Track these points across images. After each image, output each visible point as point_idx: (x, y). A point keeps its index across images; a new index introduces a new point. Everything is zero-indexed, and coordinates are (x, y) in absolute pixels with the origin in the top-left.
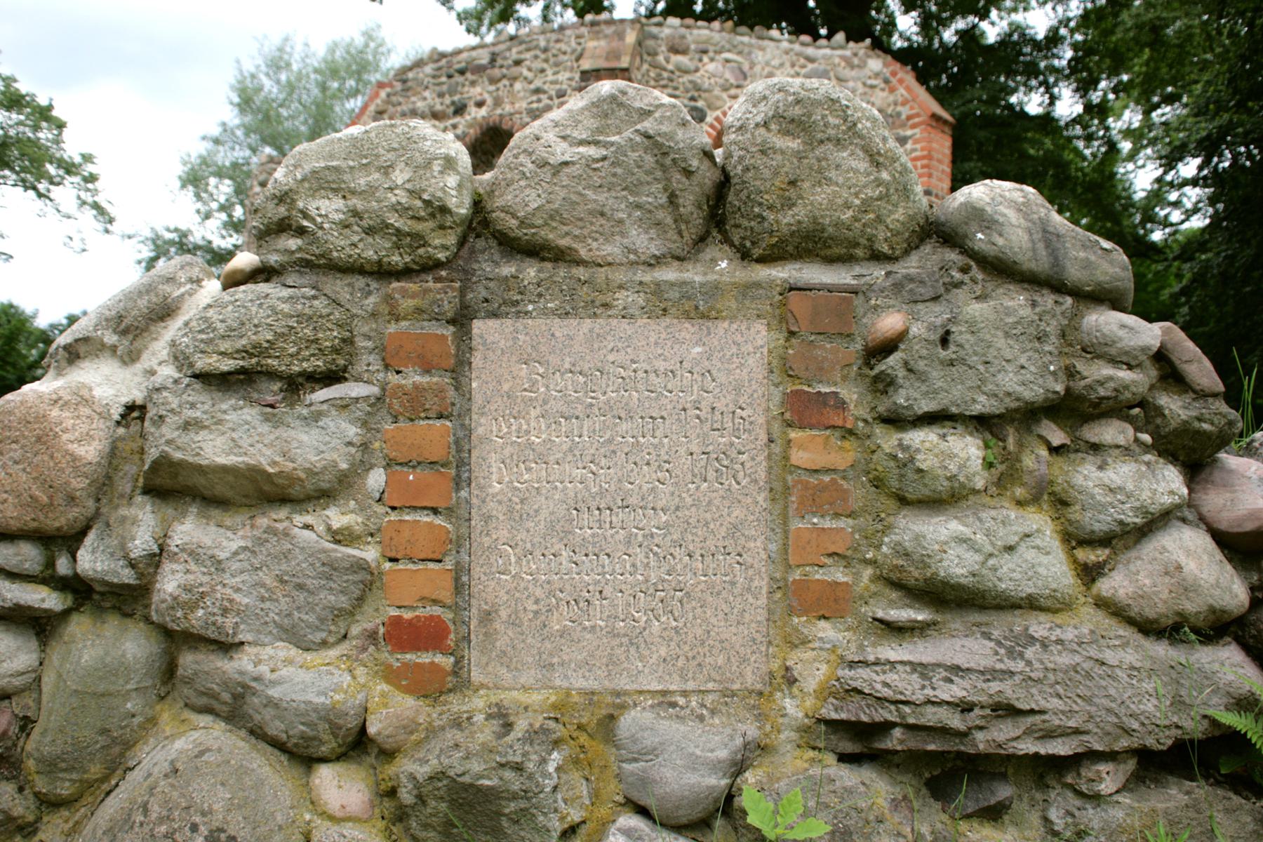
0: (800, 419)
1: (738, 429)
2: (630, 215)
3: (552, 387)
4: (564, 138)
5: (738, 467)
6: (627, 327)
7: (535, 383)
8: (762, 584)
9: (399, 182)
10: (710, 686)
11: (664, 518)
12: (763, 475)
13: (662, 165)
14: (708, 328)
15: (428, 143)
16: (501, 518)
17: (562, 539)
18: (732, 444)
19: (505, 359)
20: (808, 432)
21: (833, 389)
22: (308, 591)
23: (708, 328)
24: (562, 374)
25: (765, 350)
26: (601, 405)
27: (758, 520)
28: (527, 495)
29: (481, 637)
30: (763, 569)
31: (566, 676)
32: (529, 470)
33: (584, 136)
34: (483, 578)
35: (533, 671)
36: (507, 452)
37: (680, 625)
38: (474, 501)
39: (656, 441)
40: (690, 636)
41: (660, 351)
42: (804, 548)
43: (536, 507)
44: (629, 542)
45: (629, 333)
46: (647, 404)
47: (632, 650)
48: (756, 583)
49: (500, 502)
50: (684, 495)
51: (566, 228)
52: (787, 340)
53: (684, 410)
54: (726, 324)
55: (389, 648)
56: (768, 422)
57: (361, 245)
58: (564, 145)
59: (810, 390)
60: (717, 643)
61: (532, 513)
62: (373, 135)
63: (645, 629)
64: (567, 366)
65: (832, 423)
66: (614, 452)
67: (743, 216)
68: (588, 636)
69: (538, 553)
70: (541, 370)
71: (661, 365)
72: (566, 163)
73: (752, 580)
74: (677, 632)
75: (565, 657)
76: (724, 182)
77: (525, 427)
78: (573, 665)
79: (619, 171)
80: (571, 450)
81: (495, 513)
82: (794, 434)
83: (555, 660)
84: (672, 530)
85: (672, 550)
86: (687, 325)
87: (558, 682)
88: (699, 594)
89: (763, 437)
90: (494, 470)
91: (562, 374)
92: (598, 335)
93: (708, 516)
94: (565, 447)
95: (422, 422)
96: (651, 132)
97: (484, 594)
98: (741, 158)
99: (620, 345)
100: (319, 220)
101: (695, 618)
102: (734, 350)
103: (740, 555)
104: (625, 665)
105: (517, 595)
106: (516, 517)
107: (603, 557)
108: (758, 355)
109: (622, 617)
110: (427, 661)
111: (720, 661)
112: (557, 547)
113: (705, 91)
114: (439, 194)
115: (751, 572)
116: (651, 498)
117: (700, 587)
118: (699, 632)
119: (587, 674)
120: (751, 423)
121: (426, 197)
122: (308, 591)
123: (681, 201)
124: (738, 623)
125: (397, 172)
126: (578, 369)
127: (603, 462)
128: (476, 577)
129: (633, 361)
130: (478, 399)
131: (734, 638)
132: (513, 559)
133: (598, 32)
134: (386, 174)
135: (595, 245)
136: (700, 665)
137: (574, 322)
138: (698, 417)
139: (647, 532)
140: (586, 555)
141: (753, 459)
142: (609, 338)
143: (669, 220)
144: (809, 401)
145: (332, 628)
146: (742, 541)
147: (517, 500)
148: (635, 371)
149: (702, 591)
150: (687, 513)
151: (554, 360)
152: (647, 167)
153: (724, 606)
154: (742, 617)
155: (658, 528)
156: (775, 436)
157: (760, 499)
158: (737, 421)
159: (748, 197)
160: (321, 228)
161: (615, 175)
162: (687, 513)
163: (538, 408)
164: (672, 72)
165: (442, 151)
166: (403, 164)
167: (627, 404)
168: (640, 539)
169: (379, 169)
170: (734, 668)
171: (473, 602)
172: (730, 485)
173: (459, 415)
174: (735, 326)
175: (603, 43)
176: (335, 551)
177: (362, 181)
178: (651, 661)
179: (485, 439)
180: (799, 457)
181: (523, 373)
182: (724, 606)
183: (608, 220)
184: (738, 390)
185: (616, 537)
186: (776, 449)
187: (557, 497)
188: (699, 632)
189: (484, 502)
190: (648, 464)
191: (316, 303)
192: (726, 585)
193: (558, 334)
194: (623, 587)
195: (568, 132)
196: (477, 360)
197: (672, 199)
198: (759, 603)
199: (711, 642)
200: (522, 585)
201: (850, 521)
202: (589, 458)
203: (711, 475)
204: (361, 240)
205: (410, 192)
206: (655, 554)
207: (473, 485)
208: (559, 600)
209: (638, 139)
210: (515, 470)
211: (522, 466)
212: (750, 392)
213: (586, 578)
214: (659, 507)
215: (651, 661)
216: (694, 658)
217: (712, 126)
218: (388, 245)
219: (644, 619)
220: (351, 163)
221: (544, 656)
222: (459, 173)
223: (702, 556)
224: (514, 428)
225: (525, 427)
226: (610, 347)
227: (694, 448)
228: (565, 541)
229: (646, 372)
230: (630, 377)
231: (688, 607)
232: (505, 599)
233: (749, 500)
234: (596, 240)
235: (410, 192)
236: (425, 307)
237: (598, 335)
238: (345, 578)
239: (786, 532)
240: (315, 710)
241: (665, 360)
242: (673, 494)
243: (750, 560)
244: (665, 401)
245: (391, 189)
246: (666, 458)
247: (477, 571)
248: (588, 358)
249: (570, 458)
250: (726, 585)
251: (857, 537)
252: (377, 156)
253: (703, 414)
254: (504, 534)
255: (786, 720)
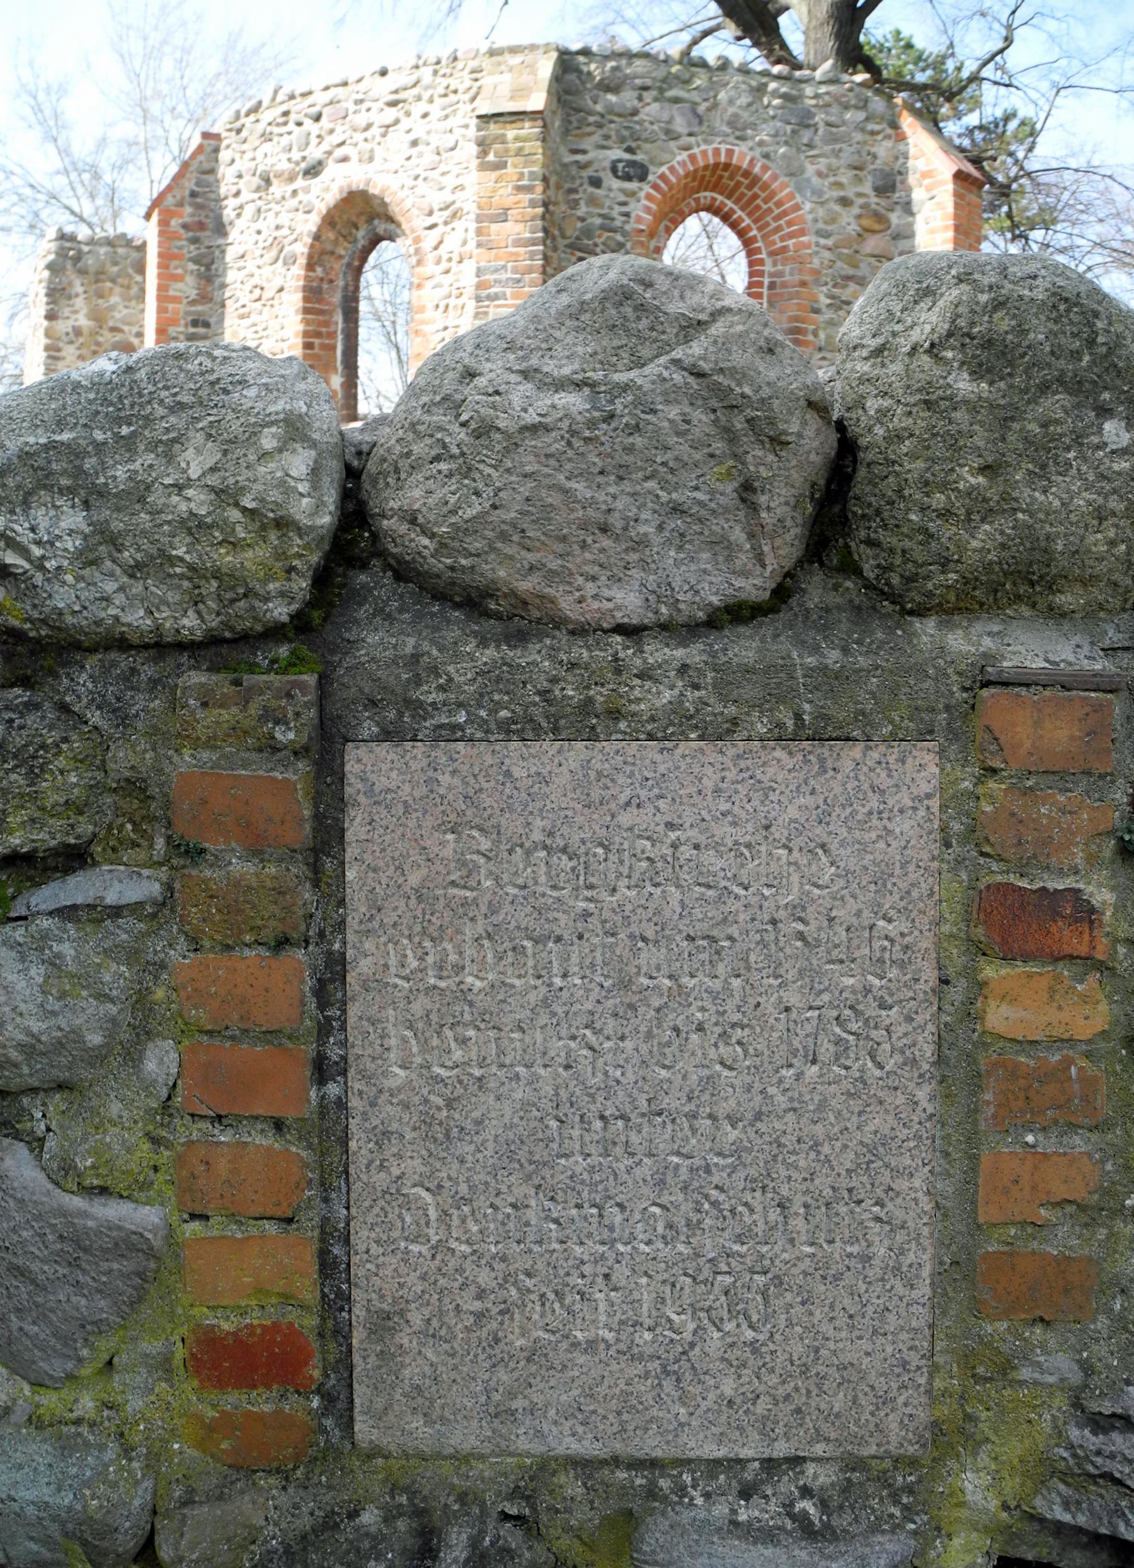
0: (1004, 942)
1: (881, 961)
2: (660, 528)
3: (506, 877)
4: (526, 374)
5: (878, 1034)
6: (658, 757)
7: (471, 870)
8: (922, 1258)
9: (194, 472)
10: (819, 1449)
11: (733, 1135)
12: (929, 1050)
13: (727, 430)
14: (822, 761)
15: (252, 392)
16: (409, 1136)
17: (529, 1177)
18: (867, 990)
19: (412, 824)
20: (1021, 968)
21: (1069, 882)
22: (33, 1281)
23: (822, 761)
24: (528, 853)
25: (935, 804)
26: (606, 914)
27: (917, 1137)
28: (460, 1090)
29: (372, 1360)
30: (926, 1231)
31: (539, 1434)
32: (463, 1042)
33: (566, 371)
34: (375, 1250)
35: (475, 1424)
36: (418, 1007)
37: (761, 1337)
38: (354, 1102)
39: (717, 985)
40: (782, 1357)
41: (724, 806)
42: (1006, 1191)
43: (476, 1114)
44: (663, 1182)
45: (662, 769)
46: (698, 913)
47: (668, 1385)
48: (911, 1257)
49: (406, 1106)
50: (772, 1090)
51: (532, 557)
52: (979, 781)
53: (774, 922)
54: (857, 750)
55: (195, 1383)
56: (938, 946)
57: (120, 599)
58: (528, 388)
59: (1023, 883)
60: (832, 1371)
61: (469, 1125)
62: (142, 374)
63: (692, 1345)
64: (537, 836)
65: (1067, 950)
66: (632, 1007)
67: (885, 527)
68: (582, 1359)
69: (482, 1202)
70: (485, 844)
71: (724, 831)
72: (533, 429)
73: (902, 1252)
74: (755, 1351)
75: (537, 1398)
76: (847, 447)
77: (453, 958)
78: (552, 1413)
79: (638, 440)
80: (545, 1003)
81: (395, 1126)
82: (990, 971)
83: (519, 1404)
84: (748, 1158)
85: (748, 1197)
86: (778, 753)
87: (523, 1444)
88: (800, 1280)
89: (930, 975)
90: (393, 1042)
91: (528, 853)
92: (599, 774)
93: (819, 1130)
94: (532, 997)
95: (247, 952)
96: (705, 366)
97: (376, 1281)
98: (882, 413)
99: (643, 794)
100: (37, 552)
101: (790, 1324)
102: (874, 803)
103: (879, 1203)
104: (654, 1412)
105: (442, 1282)
106: (438, 1133)
107: (612, 1211)
108: (922, 813)
109: (648, 1322)
110: (267, 1408)
111: (839, 1402)
112: (520, 1191)
113: (646, 140)
114: (274, 495)
115: (900, 1237)
116: (706, 1097)
117: (802, 1266)
118: (797, 1349)
119: (580, 1429)
120: (906, 948)
121: (248, 502)
122: (33, 1281)
123: (763, 499)
124: (875, 1332)
125: (190, 454)
126: (561, 843)
127: (611, 1026)
128: (361, 1248)
129: (670, 826)
130: (357, 908)
131: (866, 1361)
132: (433, 1213)
133: (499, 64)
134: (170, 458)
135: (590, 588)
136: (798, 1411)
137: (549, 747)
138: (801, 936)
139: (697, 1162)
140: (579, 1206)
141: (909, 1019)
142: (621, 780)
143: (738, 535)
144: (1022, 906)
145: (85, 1353)
146: (886, 1177)
147: (440, 1102)
148: (674, 846)
149: (805, 1274)
150: (778, 1125)
151: (511, 825)
152: (697, 433)
153: (847, 1302)
154: (882, 1320)
155: (719, 1154)
156: (951, 971)
157: (922, 1094)
158: (877, 944)
159: (900, 491)
160: (41, 568)
161: (630, 449)
162: (778, 1125)
163: (481, 922)
164: (602, 116)
165: (279, 407)
166: (200, 437)
167: (658, 912)
168: (684, 1174)
169: (153, 446)
170: (866, 1416)
171: (356, 1294)
172: (862, 1070)
173: (321, 934)
174: (875, 755)
175: (507, 77)
176: (85, 1214)
177: (120, 472)
178: (704, 1405)
179: (375, 984)
180: (999, 1017)
181: (448, 852)
182: (847, 1302)
183: (617, 538)
184: (880, 882)
185: (637, 1171)
186: (957, 993)
187: (518, 1095)
188: (797, 1349)
189: (373, 1104)
190: (700, 1028)
191: (32, 720)
192: (853, 1263)
193: (517, 772)
194: (650, 1266)
195: (534, 361)
196: (355, 829)
197: (747, 490)
198: (916, 1294)
199: (822, 1369)
200: (453, 1263)
201: (1095, 1137)
202: (583, 1019)
203: (826, 1049)
204: (121, 589)
205: (218, 492)
206: (715, 1204)
207: (351, 1073)
208: (525, 1291)
209: (678, 377)
210: (435, 1042)
211: (449, 1033)
212: (903, 885)
213: (578, 1250)
214: (721, 1113)
215: (704, 1405)
216: (787, 1398)
217: (655, 187)
218: (172, 597)
219: (691, 1326)
220: (99, 436)
221: (496, 1397)
222: (314, 445)
223: (806, 1206)
224: (430, 959)
225: (453, 958)
226: (623, 798)
227: (793, 998)
228: (537, 1181)
229: (696, 847)
230: (663, 858)
231: (777, 1303)
232: (419, 1289)
233: (900, 1099)
234: (594, 578)
235: (218, 492)
236: (247, 723)
237: (599, 774)
238: (105, 1266)
239: (974, 1159)
240: (54, 1519)
241: (734, 824)
242: (749, 1088)
243: (899, 1214)
244: (733, 906)
245: (179, 488)
246: (736, 1017)
247: (361, 1237)
248: (579, 819)
249: (543, 1019)
250: (853, 1263)
251: (1109, 1167)
252: (148, 420)
253: (810, 930)
254: (414, 1166)
255: (964, 1513)
